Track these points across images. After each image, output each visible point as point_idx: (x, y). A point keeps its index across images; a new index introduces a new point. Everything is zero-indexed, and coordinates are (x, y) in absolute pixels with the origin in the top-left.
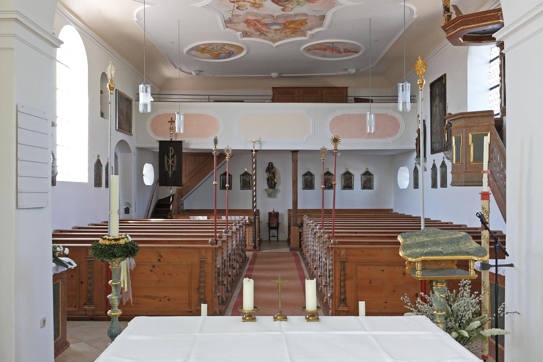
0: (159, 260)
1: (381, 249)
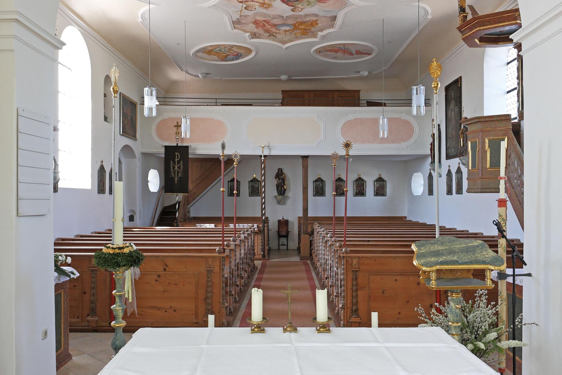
0: (165, 270)
1: (394, 258)
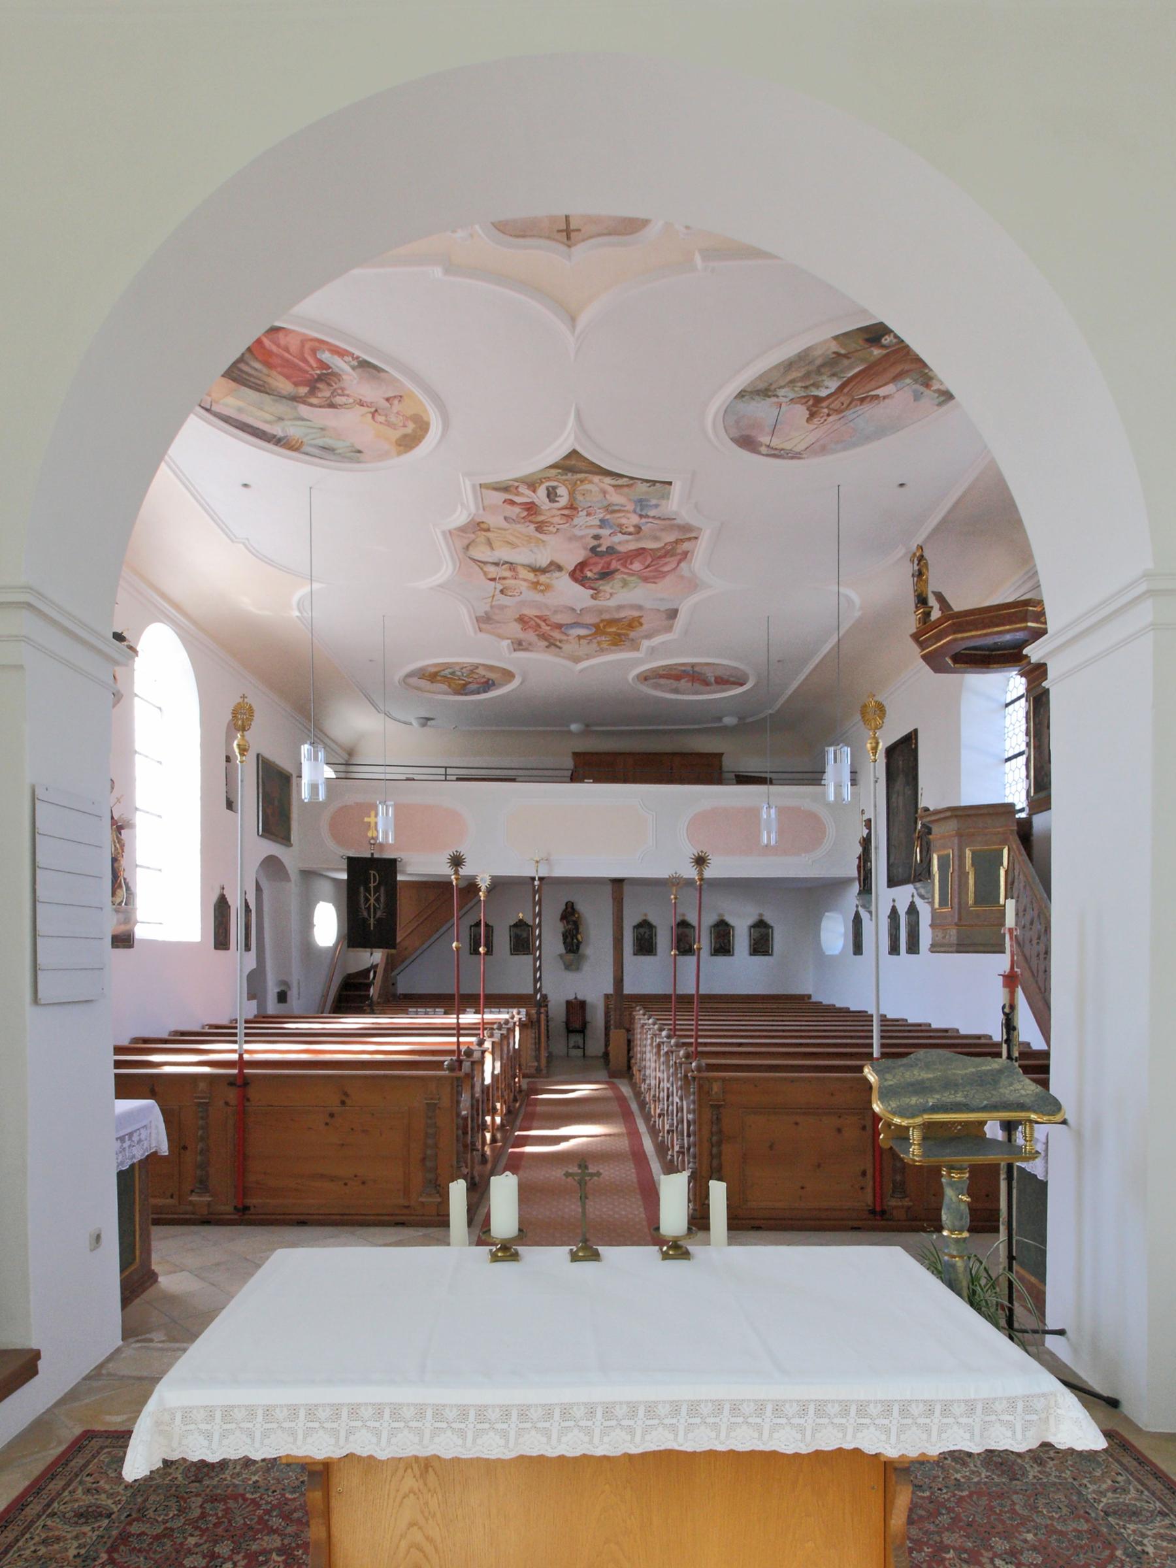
0: (343, 1103)
1: (793, 1080)
